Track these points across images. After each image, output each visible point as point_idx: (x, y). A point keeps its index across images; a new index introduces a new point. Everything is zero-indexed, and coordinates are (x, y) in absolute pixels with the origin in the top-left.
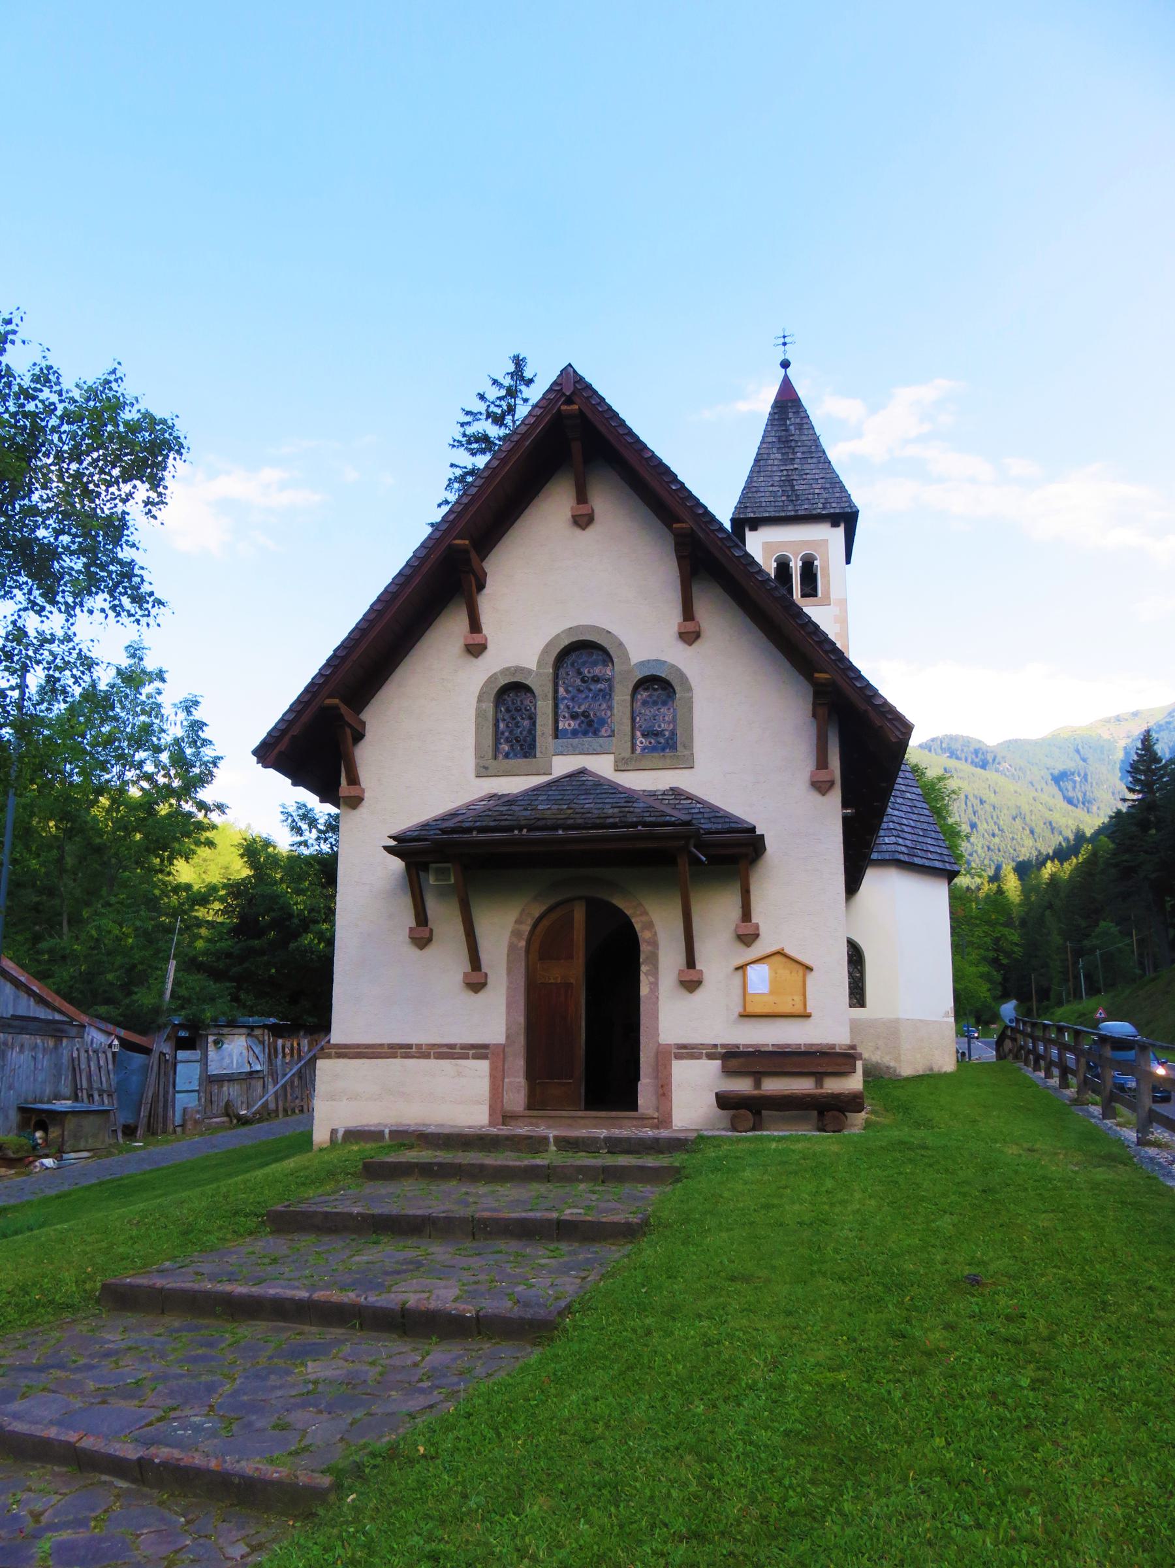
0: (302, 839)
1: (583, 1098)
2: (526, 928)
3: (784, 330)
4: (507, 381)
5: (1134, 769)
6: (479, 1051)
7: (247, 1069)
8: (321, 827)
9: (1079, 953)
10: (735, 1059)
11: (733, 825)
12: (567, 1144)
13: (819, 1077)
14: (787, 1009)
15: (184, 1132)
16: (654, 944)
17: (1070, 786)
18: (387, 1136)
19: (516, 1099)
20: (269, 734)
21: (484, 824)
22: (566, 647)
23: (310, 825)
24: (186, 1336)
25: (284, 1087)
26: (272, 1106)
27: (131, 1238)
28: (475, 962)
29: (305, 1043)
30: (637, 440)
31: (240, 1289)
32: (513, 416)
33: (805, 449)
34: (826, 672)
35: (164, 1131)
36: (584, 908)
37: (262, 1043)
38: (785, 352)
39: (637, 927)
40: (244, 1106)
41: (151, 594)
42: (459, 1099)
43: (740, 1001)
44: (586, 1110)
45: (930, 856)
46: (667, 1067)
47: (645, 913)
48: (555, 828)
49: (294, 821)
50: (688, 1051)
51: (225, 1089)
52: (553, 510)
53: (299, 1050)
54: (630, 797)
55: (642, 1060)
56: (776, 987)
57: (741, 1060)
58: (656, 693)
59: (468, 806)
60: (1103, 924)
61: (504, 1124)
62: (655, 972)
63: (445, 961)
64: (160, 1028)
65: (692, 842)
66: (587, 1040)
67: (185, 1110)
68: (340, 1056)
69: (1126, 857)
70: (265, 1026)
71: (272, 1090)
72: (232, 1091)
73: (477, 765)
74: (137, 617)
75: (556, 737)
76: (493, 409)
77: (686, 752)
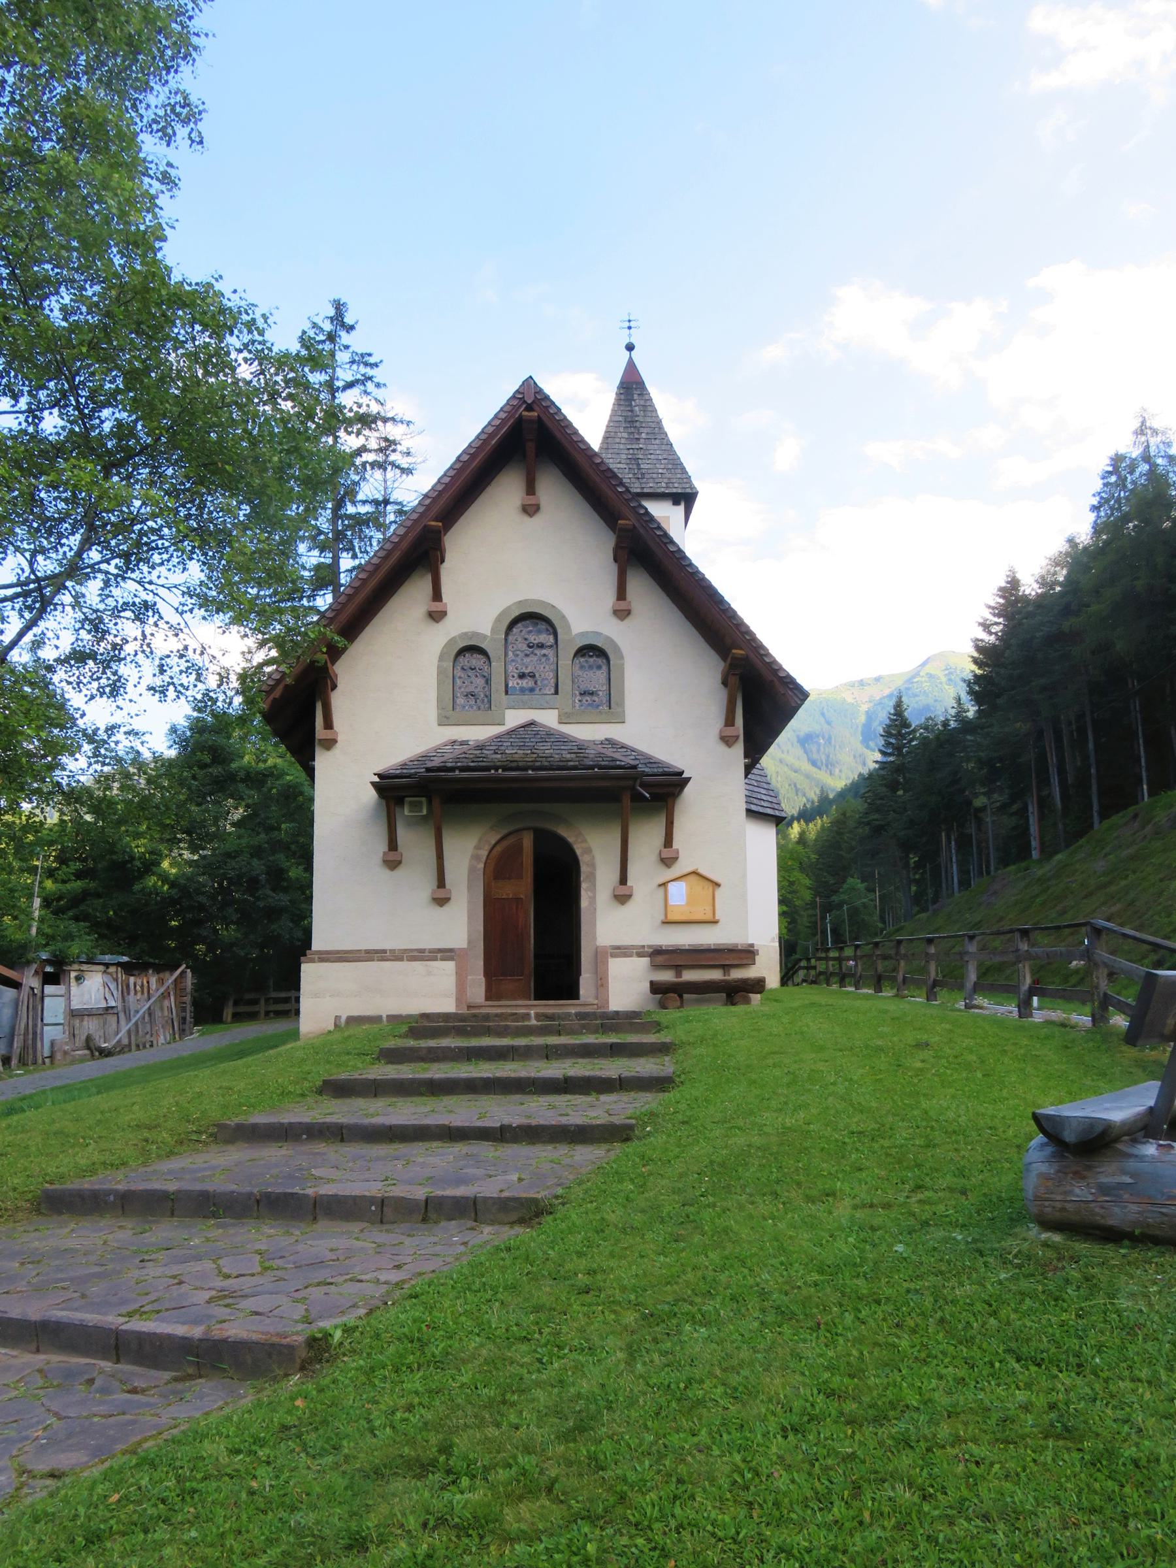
2: (484, 853)
3: (629, 314)
4: (328, 327)
5: (888, 733)
6: (446, 954)
7: (104, 1005)
9: (828, 908)
10: (659, 956)
13: (726, 968)
15: (52, 1062)
16: (593, 865)
18: (385, 1019)
19: (477, 991)
23: (139, 769)
25: (136, 1024)
28: (441, 882)
29: (153, 980)
33: (649, 430)
35: (35, 1063)
37: (116, 980)
38: (630, 335)
39: (578, 852)
42: (436, 991)
44: (535, 999)
45: (763, 803)
47: (585, 841)
48: (526, 769)
50: (622, 951)
51: (85, 1023)
54: (581, 747)
56: (691, 899)
57: (666, 956)
58: (591, 660)
59: (436, 750)
63: (416, 879)
64: (29, 963)
67: (52, 1043)
68: (322, 960)
69: (876, 816)
71: (124, 1030)
72: (90, 1026)
73: (439, 715)
75: (507, 693)
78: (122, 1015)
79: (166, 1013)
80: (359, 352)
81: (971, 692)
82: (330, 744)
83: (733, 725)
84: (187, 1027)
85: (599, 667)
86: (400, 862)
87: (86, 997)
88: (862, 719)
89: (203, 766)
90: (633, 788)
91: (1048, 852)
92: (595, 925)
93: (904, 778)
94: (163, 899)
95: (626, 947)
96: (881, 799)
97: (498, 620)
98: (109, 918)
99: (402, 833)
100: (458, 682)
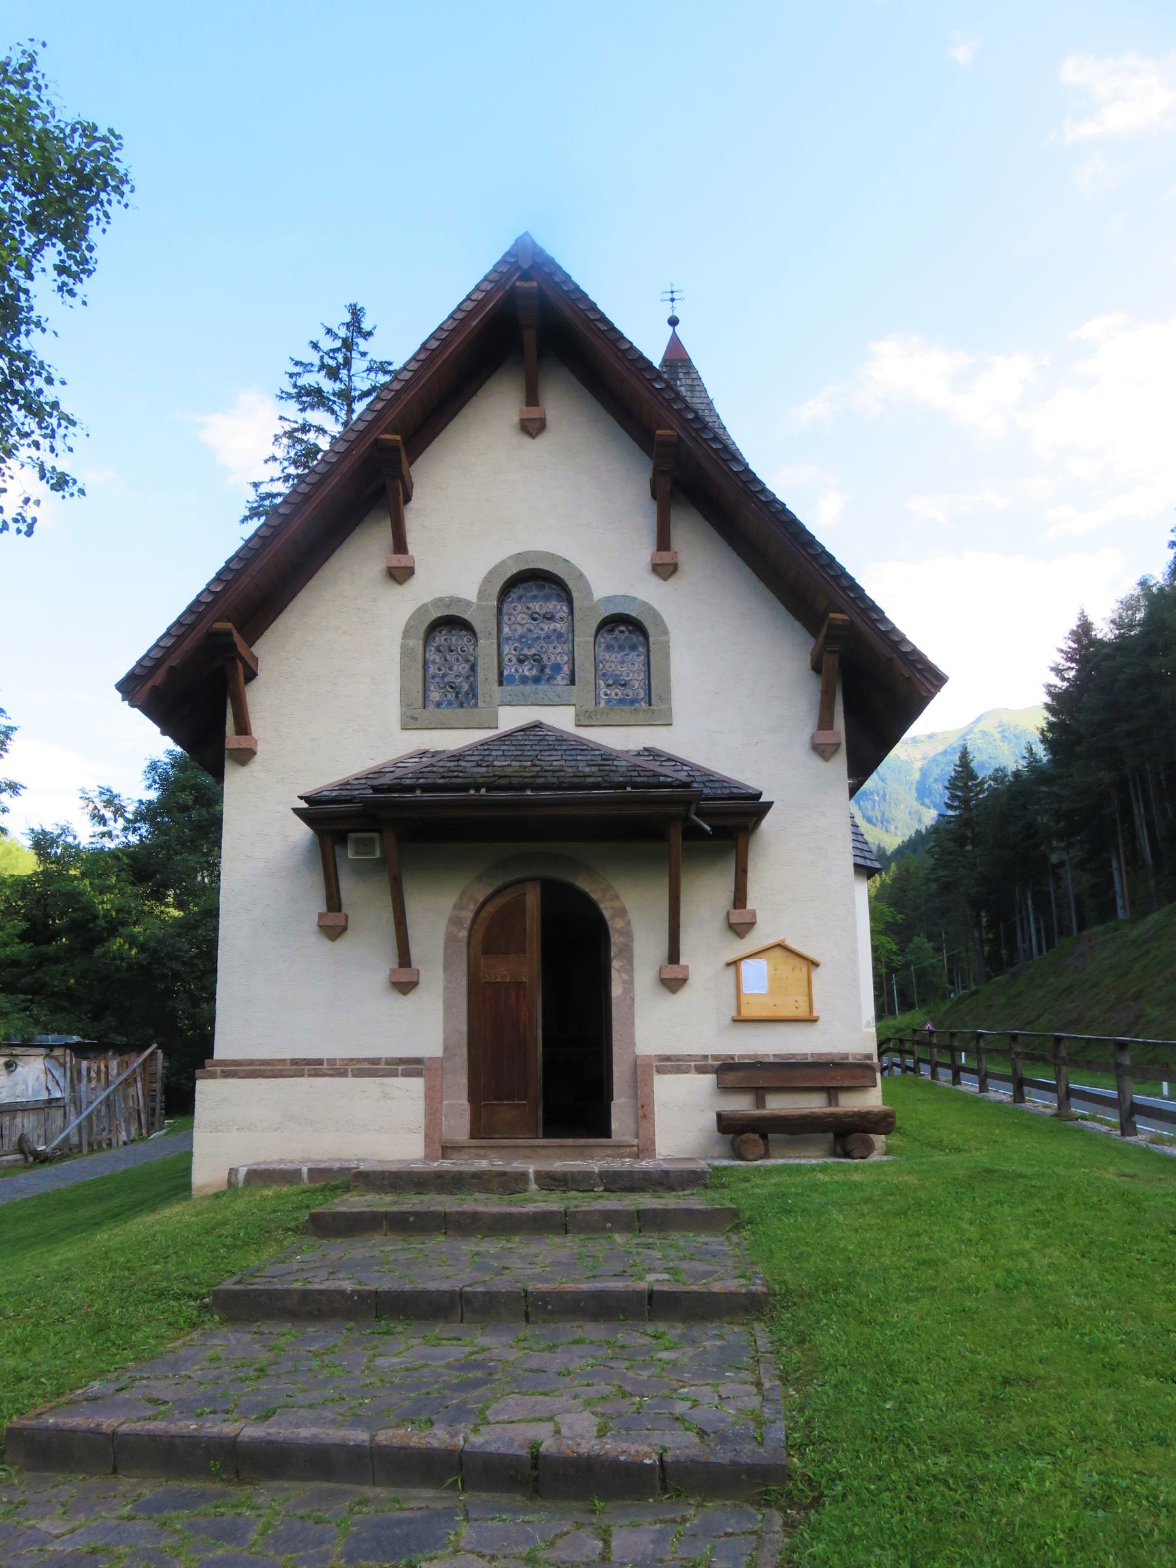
0: (105, 829)
1: (541, 1123)
2: (468, 915)
3: (672, 285)
4: (343, 332)
5: (953, 785)
6: (411, 1066)
7: (45, 1096)
8: (130, 816)
10: (731, 1073)
11: (734, 790)
12: (552, 1182)
13: (832, 1093)
14: (790, 1012)
16: (628, 934)
17: (869, 805)
19: (458, 1125)
20: (139, 664)
21: (430, 781)
22: (513, 577)
23: (115, 813)
24: (180, 1518)
25: (89, 1117)
26: (75, 1140)
27: (17, 1341)
28: (404, 958)
29: (114, 1065)
30: (612, 328)
31: (252, 1431)
32: (349, 370)
34: (842, 612)
36: (539, 889)
37: (63, 1065)
39: (607, 914)
40: (42, 1140)
41: (55, 405)
42: (388, 1127)
43: (734, 1003)
44: (545, 1136)
46: (649, 1083)
47: (617, 897)
48: (522, 787)
49: (96, 808)
50: (673, 1064)
51: (18, 1120)
52: (495, 412)
53: (107, 1074)
54: (607, 757)
55: (615, 1075)
56: (776, 986)
57: (741, 1074)
58: (623, 636)
59: (396, 764)
60: (917, 939)
61: (444, 1157)
62: (629, 968)
63: (366, 956)
65: (693, 808)
66: (547, 1053)
68: (227, 1075)
69: (945, 873)
70: (67, 1046)
71: (74, 1122)
72: (26, 1124)
73: (403, 714)
74: (35, 437)
75: (501, 683)
76: (327, 360)
77: (663, 706)
78: (71, 1109)
79: (131, 1104)
80: (378, 360)
81: (1044, 741)
82: (245, 756)
83: (831, 728)
84: (156, 1119)
85: (633, 648)
86: (344, 929)
87: (20, 1088)
88: (917, 776)
89: (184, 809)
90: (686, 818)
91: (1139, 911)
92: (633, 1024)
93: (973, 833)
94: (130, 967)
95: (679, 1058)
96: (950, 854)
97: (488, 579)
98: (69, 988)
99: (348, 886)
100: (432, 670)
